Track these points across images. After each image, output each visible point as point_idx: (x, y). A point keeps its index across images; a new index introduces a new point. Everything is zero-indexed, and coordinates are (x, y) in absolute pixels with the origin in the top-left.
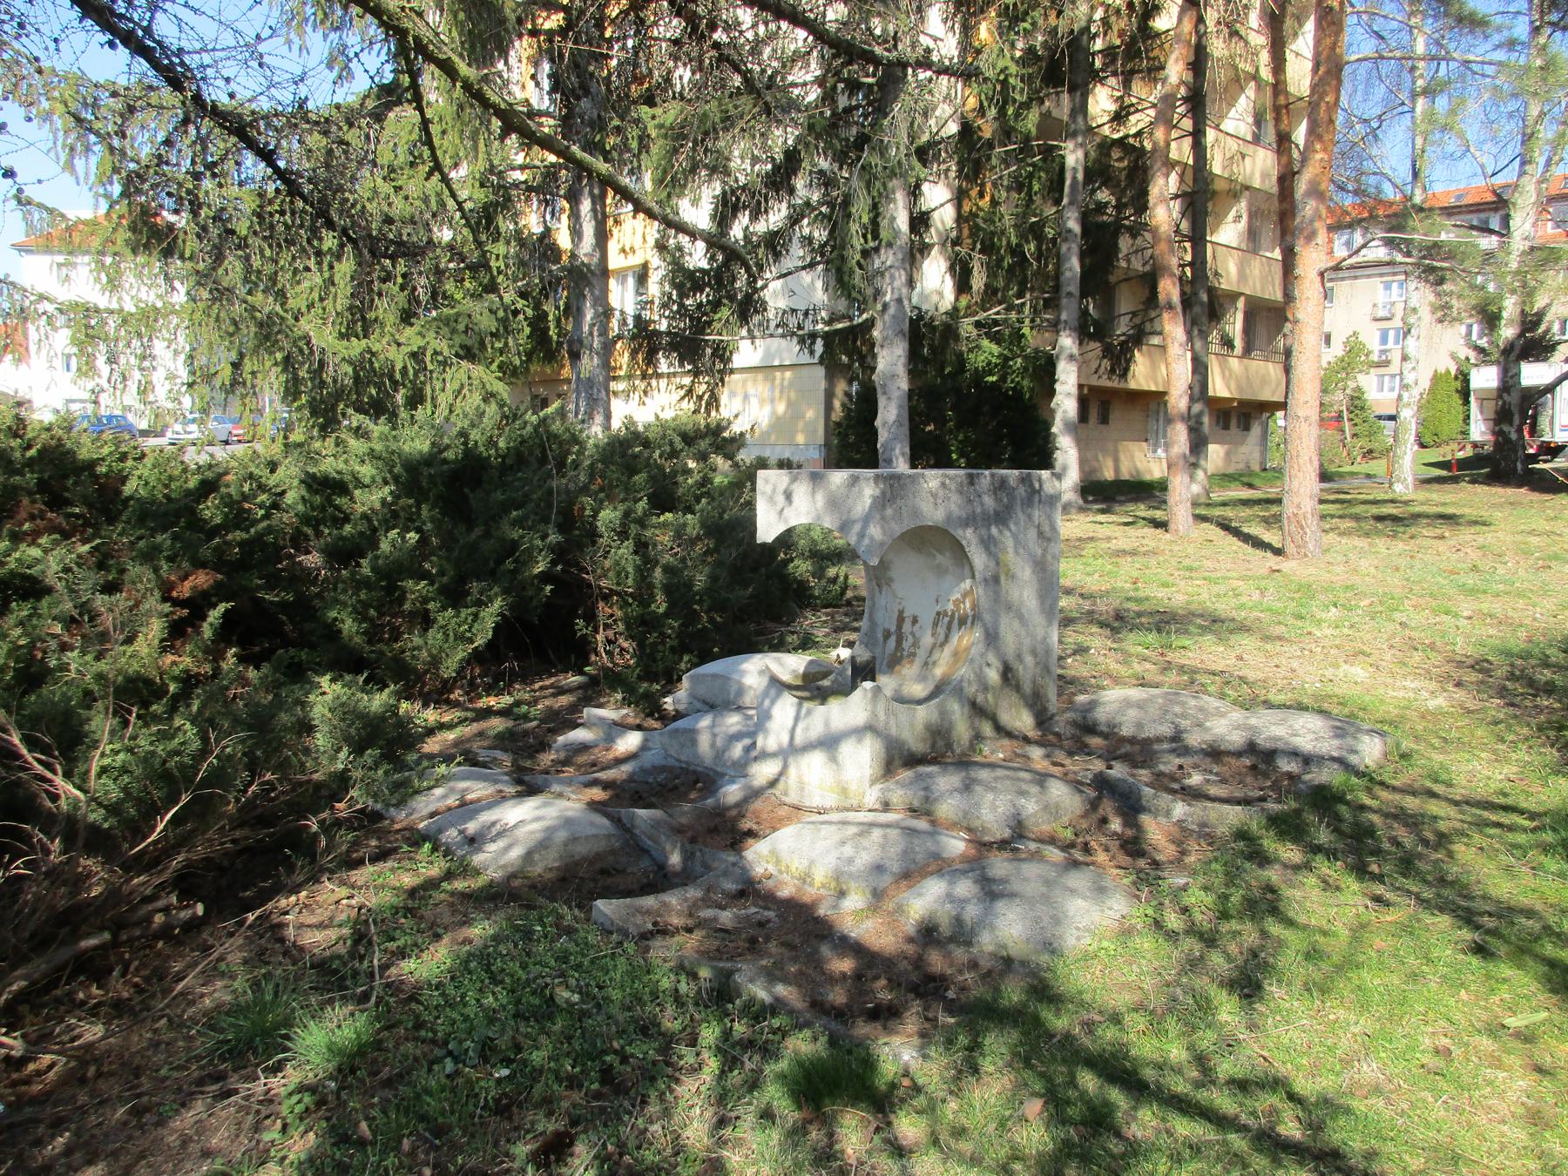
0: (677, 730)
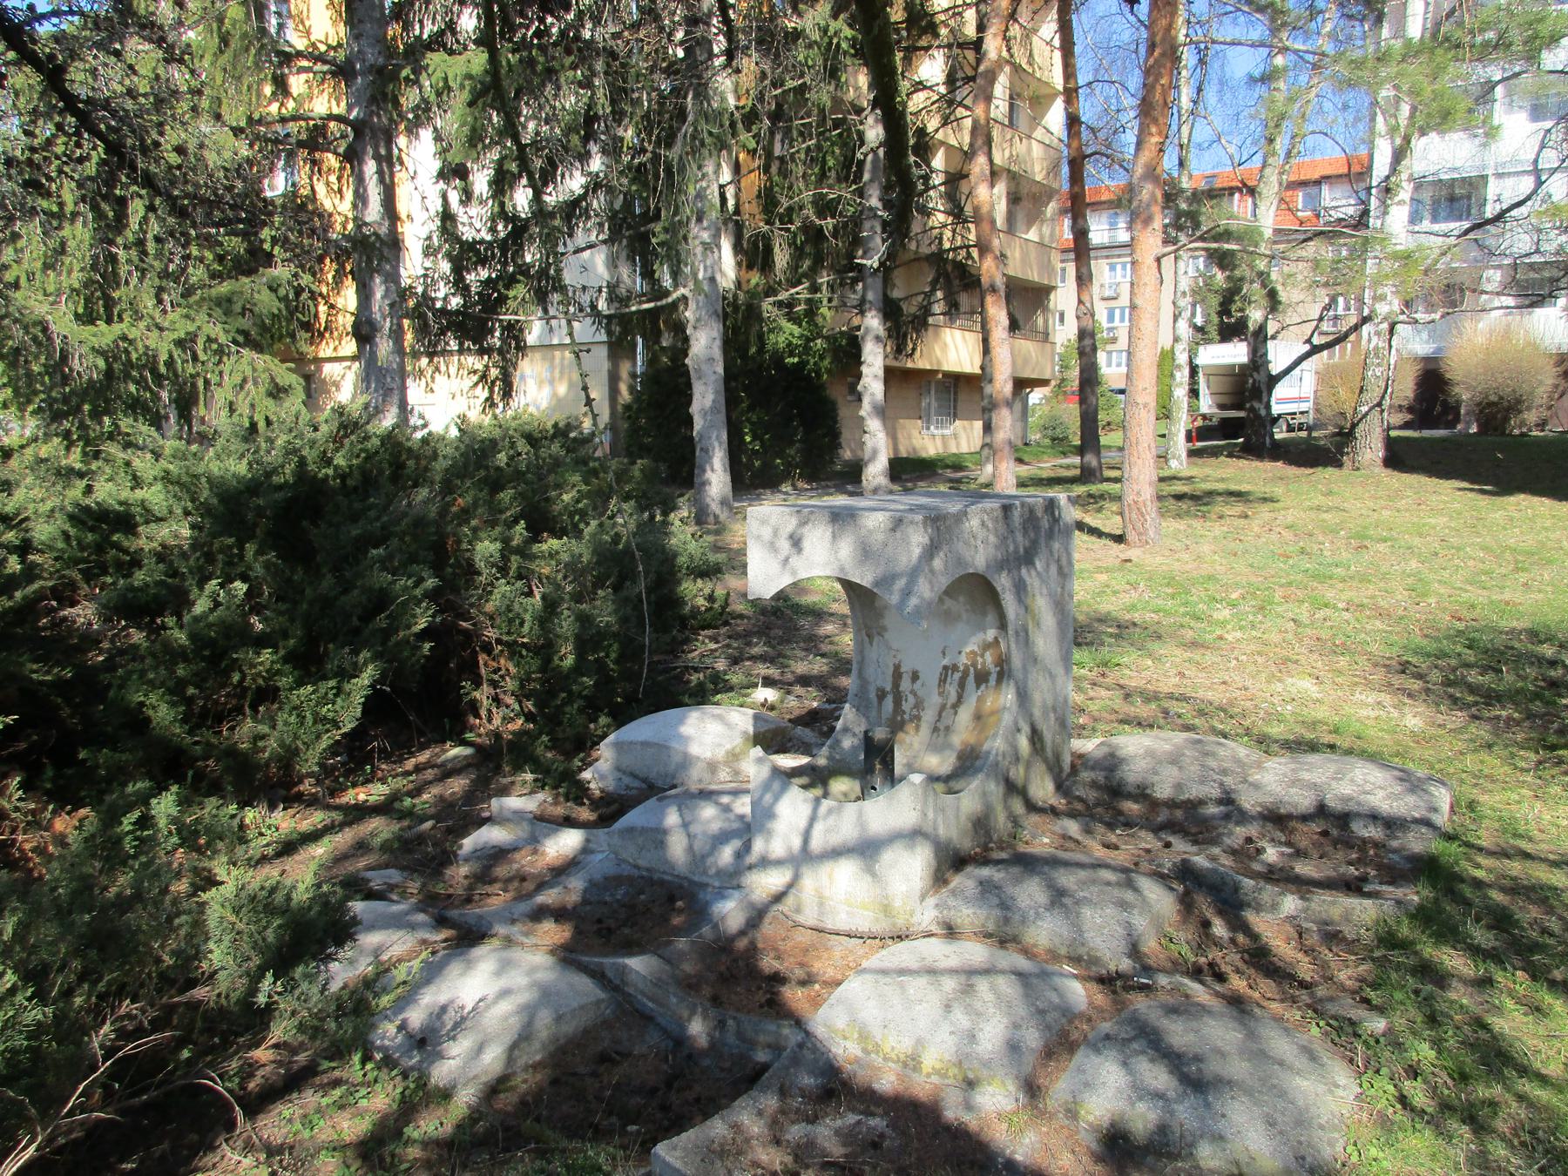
0: (631, 830)
